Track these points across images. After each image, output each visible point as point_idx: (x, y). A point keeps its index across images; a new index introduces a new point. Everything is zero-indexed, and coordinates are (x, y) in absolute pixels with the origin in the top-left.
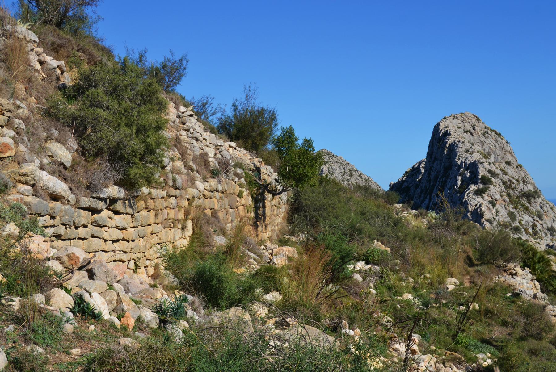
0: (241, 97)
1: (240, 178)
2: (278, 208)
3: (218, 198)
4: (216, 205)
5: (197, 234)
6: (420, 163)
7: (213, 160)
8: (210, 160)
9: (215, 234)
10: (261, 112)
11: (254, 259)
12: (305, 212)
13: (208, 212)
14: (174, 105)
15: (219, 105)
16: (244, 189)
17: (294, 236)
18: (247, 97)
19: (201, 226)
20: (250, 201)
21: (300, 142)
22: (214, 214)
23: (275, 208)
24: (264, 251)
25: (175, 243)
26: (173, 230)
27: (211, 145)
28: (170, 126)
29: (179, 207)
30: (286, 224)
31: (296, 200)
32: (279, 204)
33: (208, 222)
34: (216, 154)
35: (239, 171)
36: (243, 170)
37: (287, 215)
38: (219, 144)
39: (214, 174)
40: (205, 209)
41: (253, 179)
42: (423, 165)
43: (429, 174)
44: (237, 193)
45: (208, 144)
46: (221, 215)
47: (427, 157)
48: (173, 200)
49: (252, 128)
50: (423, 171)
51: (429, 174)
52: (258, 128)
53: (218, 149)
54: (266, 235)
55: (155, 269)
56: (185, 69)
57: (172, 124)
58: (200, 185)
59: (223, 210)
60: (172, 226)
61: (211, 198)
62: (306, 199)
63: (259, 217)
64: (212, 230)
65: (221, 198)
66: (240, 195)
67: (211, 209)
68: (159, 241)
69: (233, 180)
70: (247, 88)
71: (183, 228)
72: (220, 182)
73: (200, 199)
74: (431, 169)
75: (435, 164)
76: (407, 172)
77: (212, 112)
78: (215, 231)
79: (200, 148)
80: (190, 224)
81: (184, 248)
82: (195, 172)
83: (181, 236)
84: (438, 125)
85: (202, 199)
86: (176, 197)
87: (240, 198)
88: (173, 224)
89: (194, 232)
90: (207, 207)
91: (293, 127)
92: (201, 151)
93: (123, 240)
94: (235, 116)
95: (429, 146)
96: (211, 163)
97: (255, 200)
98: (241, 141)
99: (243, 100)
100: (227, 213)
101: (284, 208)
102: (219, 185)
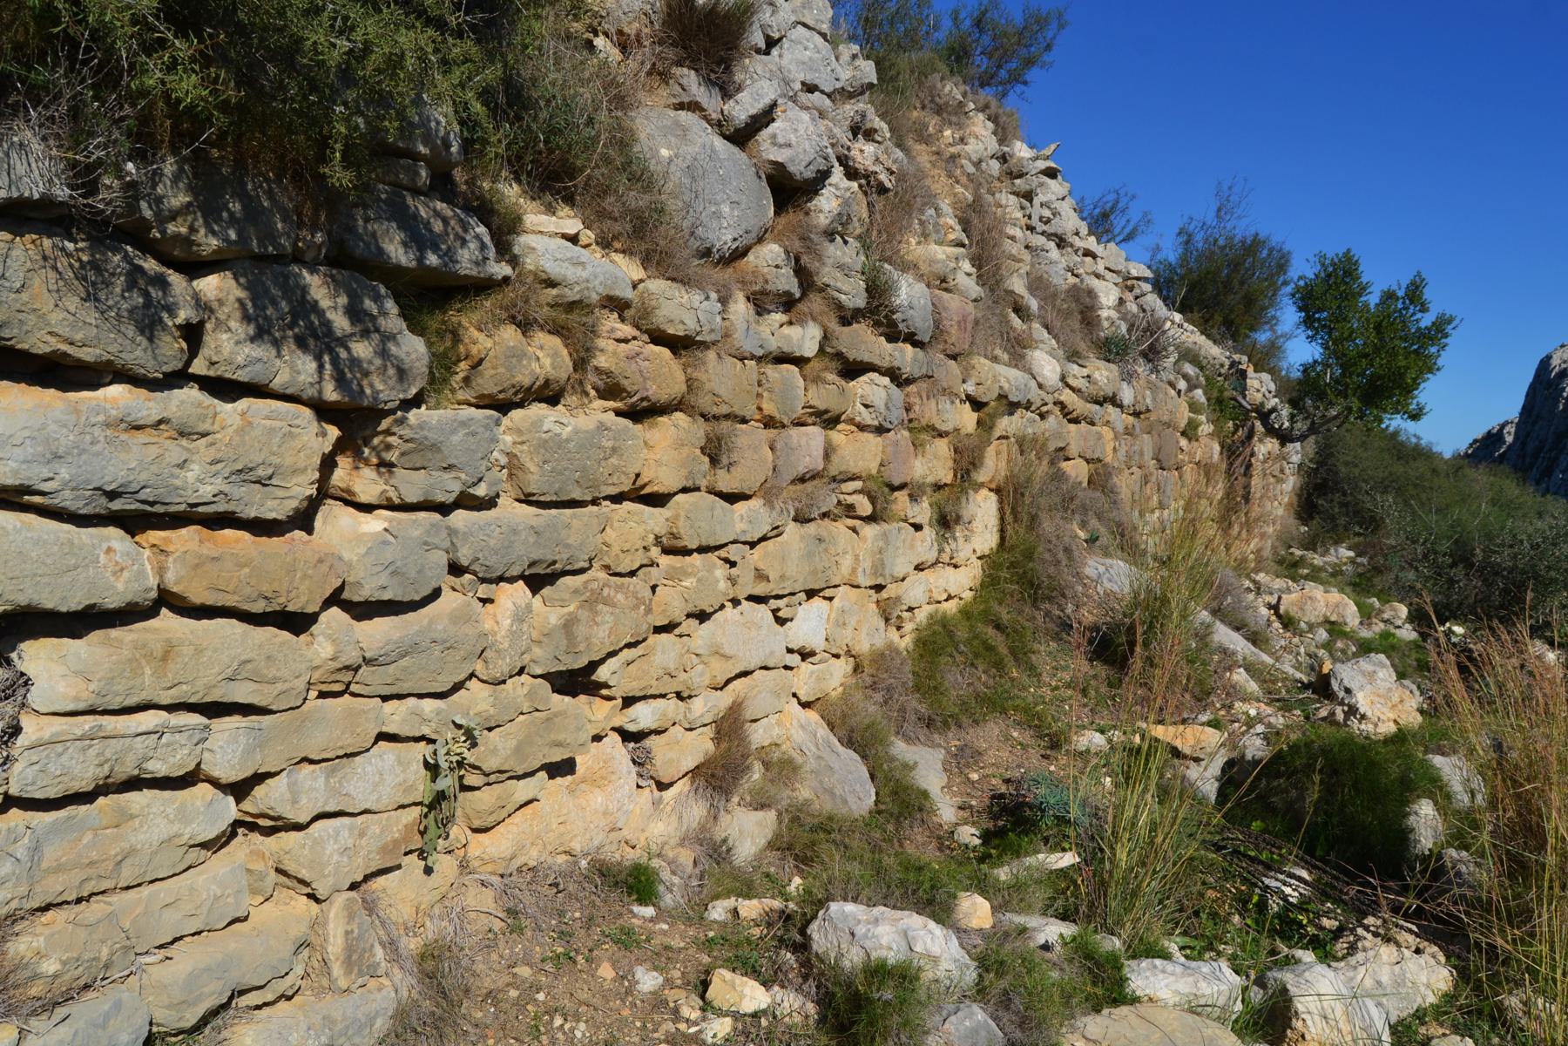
0: (1202, 210)
1: (1192, 387)
2: (1280, 481)
3: (1120, 428)
4: (1108, 446)
5: (1012, 548)
6: (1503, 426)
7: (1114, 314)
8: (1104, 313)
9: (1090, 550)
10: (1253, 247)
11: (1250, 668)
12: (1344, 494)
13: (1077, 470)
14: (990, 125)
15: (1145, 214)
16: (1203, 418)
17: (1315, 551)
18: (1219, 210)
19: (1034, 518)
20: (1214, 451)
21: (1373, 299)
22: (1100, 478)
23: (1272, 480)
24: (1251, 596)
25: (891, 591)
26: (869, 531)
27: (1109, 275)
28: (964, 172)
29: (923, 432)
30: (1292, 521)
31: (1321, 464)
32: (1282, 471)
33: (1068, 504)
34: (1121, 301)
35: (1189, 369)
36: (1202, 368)
37: (1295, 499)
38: (1134, 273)
39: (1111, 350)
40: (1062, 453)
41: (1227, 394)
42: (1511, 429)
43: (1524, 444)
44: (1183, 424)
45: (1100, 269)
46: (1125, 484)
47: (1521, 414)
48: (873, 388)
49: (1227, 285)
50: (1509, 439)
51: (1524, 444)
52: (1242, 283)
53: (1131, 289)
54: (1249, 548)
55: (718, 738)
56: (1048, 47)
57: (971, 169)
58: (1046, 363)
59: (1135, 469)
60: (865, 507)
61: (1092, 424)
62: (1347, 464)
63: (1237, 501)
64: (1082, 534)
65: (1129, 432)
66: (1190, 432)
67: (1088, 461)
68: (760, 589)
69: (1172, 385)
70: (1225, 188)
71: (946, 522)
72: (1128, 377)
73: (1042, 416)
74: (1528, 434)
75: (1537, 428)
76: (1475, 441)
77: (1127, 231)
78: (1092, 540)
79: (1070, 270)
80: (983, 510)
81: (951, 607)
82: (1036, 325)
83: (931, 556)
84: (1549, 357)
85: (1051, 419)
86: (894, 375)
87: (1190, 440)
88: (873, 500)
89: (1002, 538)
90: (1073, 450)
91: (1357, 253)
92: (1072, 280)
93: (167, 600)
94: (1184, 260)
95: (1527, 395)
96: (1106, 324)
97: (1230, 451)
98: (1196, 315)
99: (1210, 218)
100: (1146, 480)
101: (1291, 483)
102: (1125, 385)
